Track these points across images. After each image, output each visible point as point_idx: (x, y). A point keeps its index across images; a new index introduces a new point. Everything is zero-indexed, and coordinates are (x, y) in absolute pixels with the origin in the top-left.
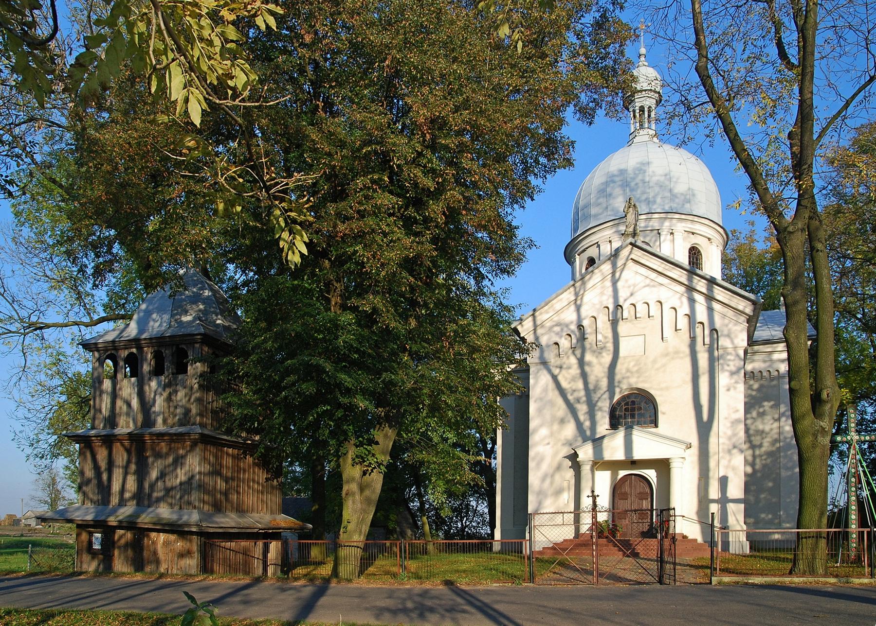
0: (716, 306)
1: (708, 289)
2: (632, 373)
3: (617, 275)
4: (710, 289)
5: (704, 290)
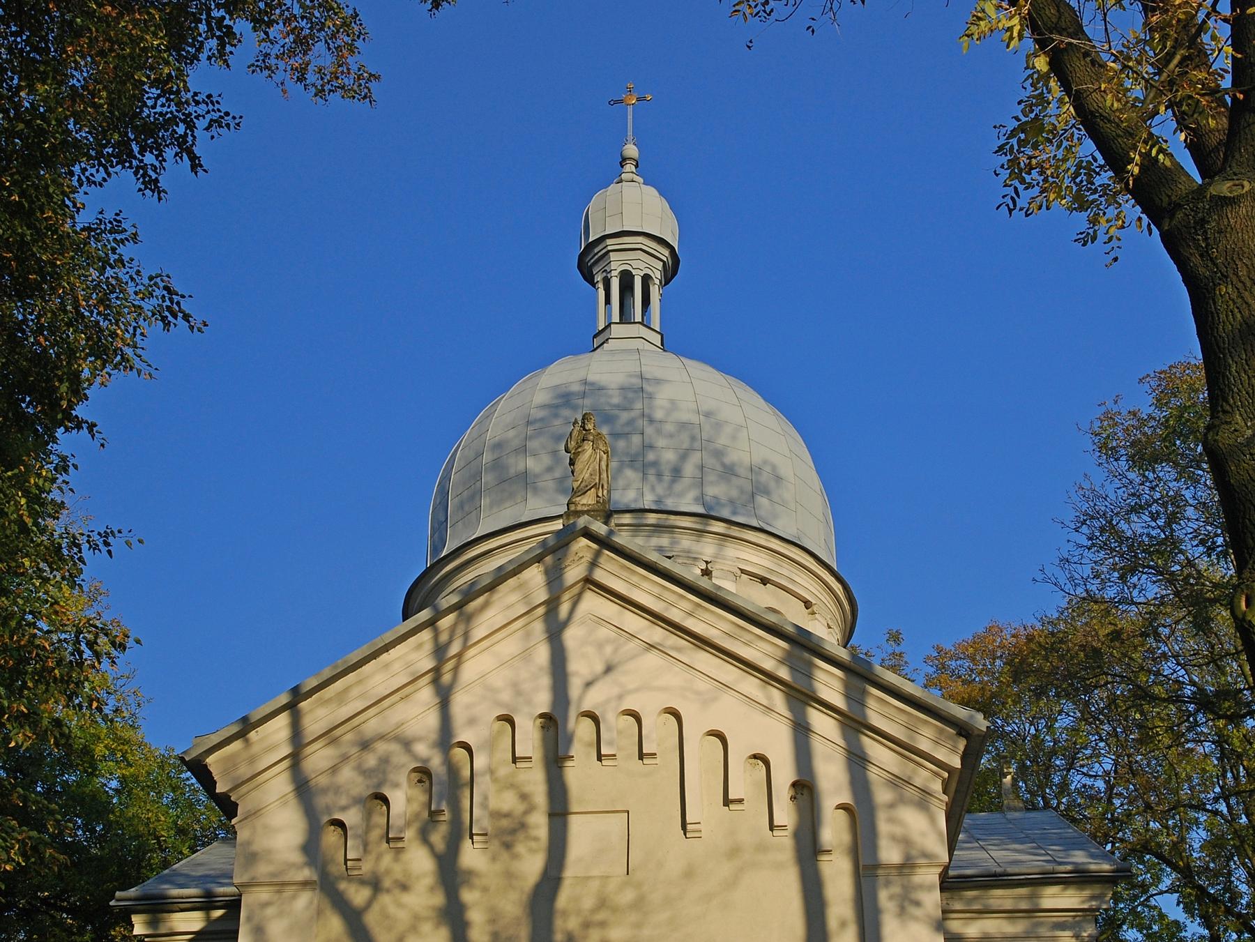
0: (877, 752)
1: (848, 697)
2: (615, 910)
3: (564, 609)
4: (855, 697)
5: (838, 701)
